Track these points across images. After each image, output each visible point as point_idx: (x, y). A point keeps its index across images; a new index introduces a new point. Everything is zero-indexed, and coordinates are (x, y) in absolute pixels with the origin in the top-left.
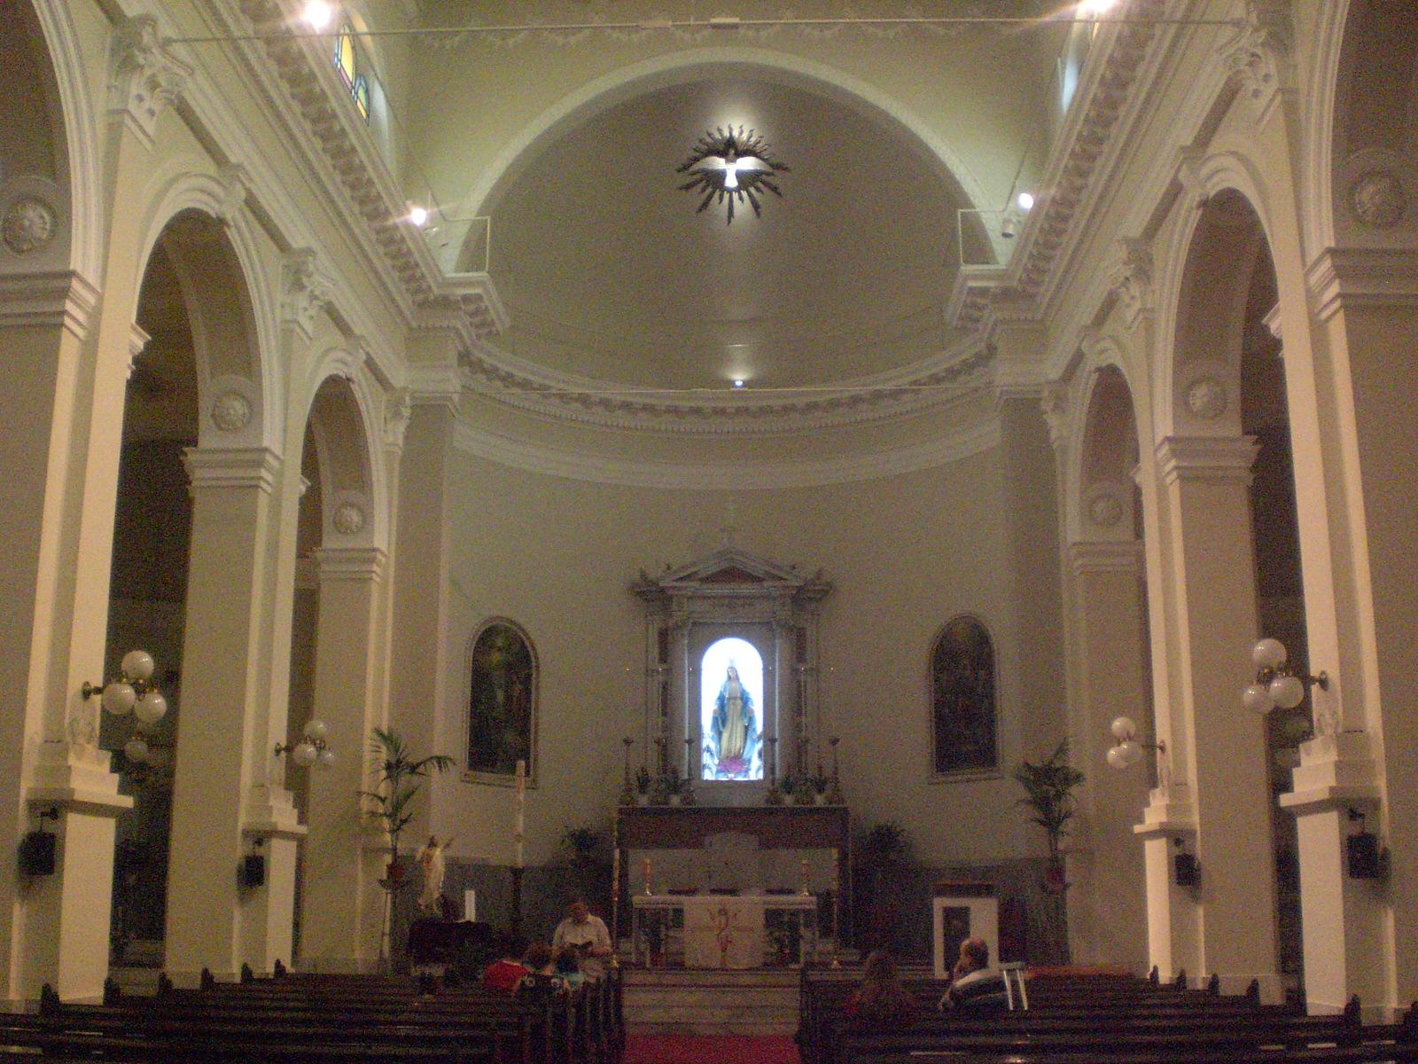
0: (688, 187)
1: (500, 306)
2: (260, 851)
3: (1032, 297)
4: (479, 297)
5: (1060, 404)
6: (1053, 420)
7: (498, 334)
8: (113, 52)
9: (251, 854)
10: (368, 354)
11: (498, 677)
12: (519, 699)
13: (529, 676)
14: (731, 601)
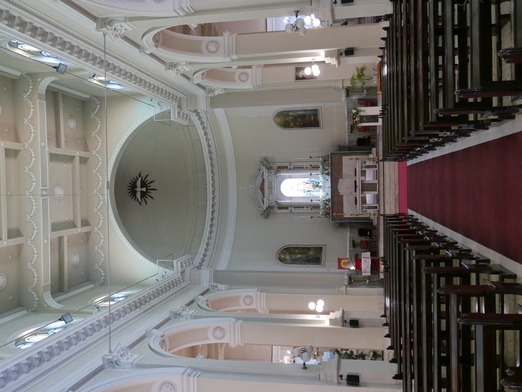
0: (146, 202)
1: (184, 257)
2: (348, 321)
3: (180, 98)
4: (181, 263)
5: (211, 91)
6: (217, 93)
7: (192, 258)
8: (113, 367)
9: (349, 324)
10: (199, 295)
11: (293, 257)
12: (300, 250)
13: (293, 248)
14: (270, 188)
